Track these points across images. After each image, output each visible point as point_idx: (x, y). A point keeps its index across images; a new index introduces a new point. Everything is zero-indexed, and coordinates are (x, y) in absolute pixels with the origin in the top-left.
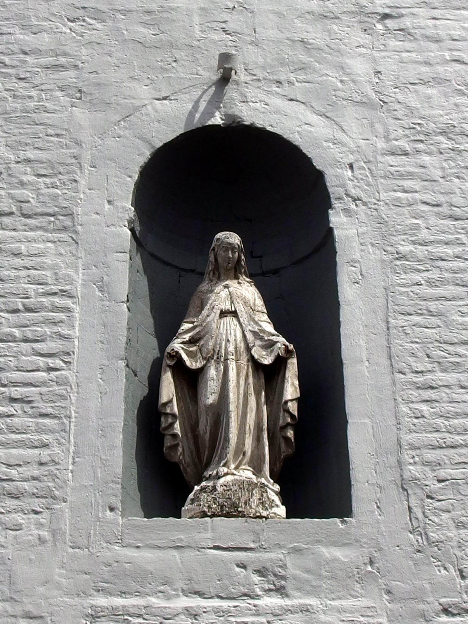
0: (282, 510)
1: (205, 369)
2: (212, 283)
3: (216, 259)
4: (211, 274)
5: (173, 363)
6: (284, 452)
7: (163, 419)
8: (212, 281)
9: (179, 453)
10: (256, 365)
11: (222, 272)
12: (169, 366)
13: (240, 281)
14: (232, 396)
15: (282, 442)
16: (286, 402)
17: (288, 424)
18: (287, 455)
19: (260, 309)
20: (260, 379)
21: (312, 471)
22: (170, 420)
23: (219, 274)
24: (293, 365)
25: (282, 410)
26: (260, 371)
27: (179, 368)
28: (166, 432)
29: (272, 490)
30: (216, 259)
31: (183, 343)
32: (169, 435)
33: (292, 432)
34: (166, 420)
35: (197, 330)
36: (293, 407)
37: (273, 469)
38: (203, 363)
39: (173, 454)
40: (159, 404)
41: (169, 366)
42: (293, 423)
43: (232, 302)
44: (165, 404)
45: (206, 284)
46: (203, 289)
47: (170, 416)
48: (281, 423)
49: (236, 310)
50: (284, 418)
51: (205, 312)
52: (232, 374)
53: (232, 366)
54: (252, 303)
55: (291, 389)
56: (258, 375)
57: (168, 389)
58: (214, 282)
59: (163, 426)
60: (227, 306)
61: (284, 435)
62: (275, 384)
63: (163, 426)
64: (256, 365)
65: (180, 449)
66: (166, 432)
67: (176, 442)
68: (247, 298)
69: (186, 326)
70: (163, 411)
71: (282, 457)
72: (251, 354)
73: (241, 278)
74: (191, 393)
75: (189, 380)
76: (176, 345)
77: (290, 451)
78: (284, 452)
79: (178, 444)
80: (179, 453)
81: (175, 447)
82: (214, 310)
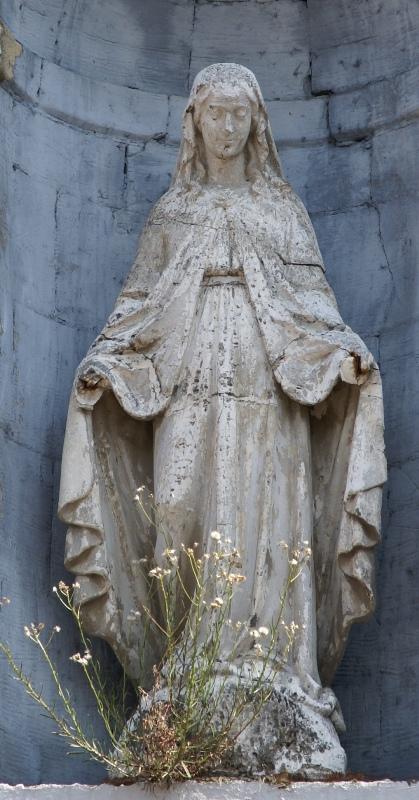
0: (333, 757)
1: (168, 414)
2: (189, 194)
3: (198, 134)
4: (188, 169)
5: (94, 402)
6: (349, 613)
7: (70, 538)
8: (189, 188)
9: (108, 618)
10: (289, 405)
11: (214, 164)
12: (84, 411)
13: (255, 188)
14: (224, 483)
15: (346, 586)
16: (353, 497)
17: (357, 549)
18: (354, 620)
19: (302, 256)
20: (296, 437)
22: (85, 543)
23: (206, 167)
25: (345, 514)
26: (298, 415)
27: (108, 412)
28: (78, 569)
29: (315, 709)
30: (198, 134)
31: (119, 352)
32: (82, 575)
33: (367, 565)
34: (78, 542)
35: (149, 321)
36: (371, 508)
37: (326, 650)
38: (163, 403)
39: (94, 619)
40: (62, 504)
41: (84, 411)
42: (372, 543)
43: (232, 249)
44: (73, 505)
45: (174, 195)
46: (167, 210)
47: (85, 532)
48: (343, 546)
49: (241, 269)
50: (350, 534)
51: (169, 274)
52: (227, 430)
53: (228, 411)
54: (281, 243)
55: (364, 461)
56: (293, 428)
57: (80, 471)
58: (194, 192)
59: (69, 556)
60: (219, 258)
61: (349, 574)
62: (334, 446)
63: (69, 556)
64: (289, 405)
65: (110, 607)
66: (78, 569)
67: (100, 593)
68: (269, 232)
69: (126, 306)
70: (70, 521)
71: (345, 624)
72: (274, 377)
73: (259, 179)
74: (140, 469)
75: (134, 438)
76: (101, 358)
77: (364, 610)
78: (349, 613)
79: (105, 597)
80: (108, 618)
81: (98, 602)
82: (191, 270)
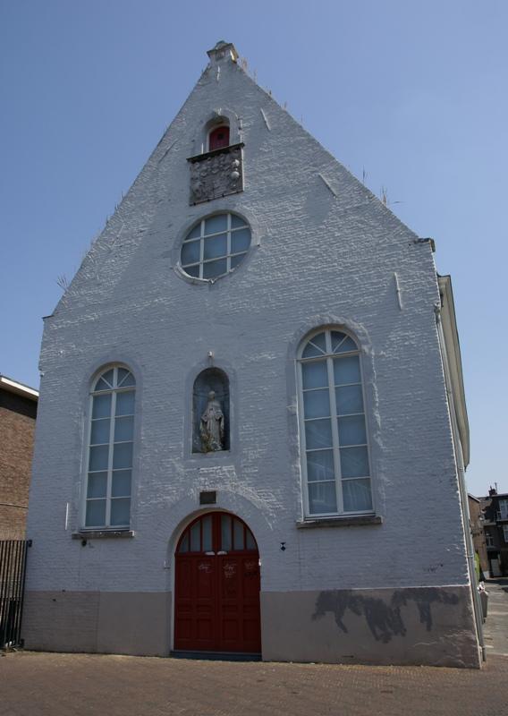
21: (225, 444)
24: (223, 419)
55: (222, 424)
